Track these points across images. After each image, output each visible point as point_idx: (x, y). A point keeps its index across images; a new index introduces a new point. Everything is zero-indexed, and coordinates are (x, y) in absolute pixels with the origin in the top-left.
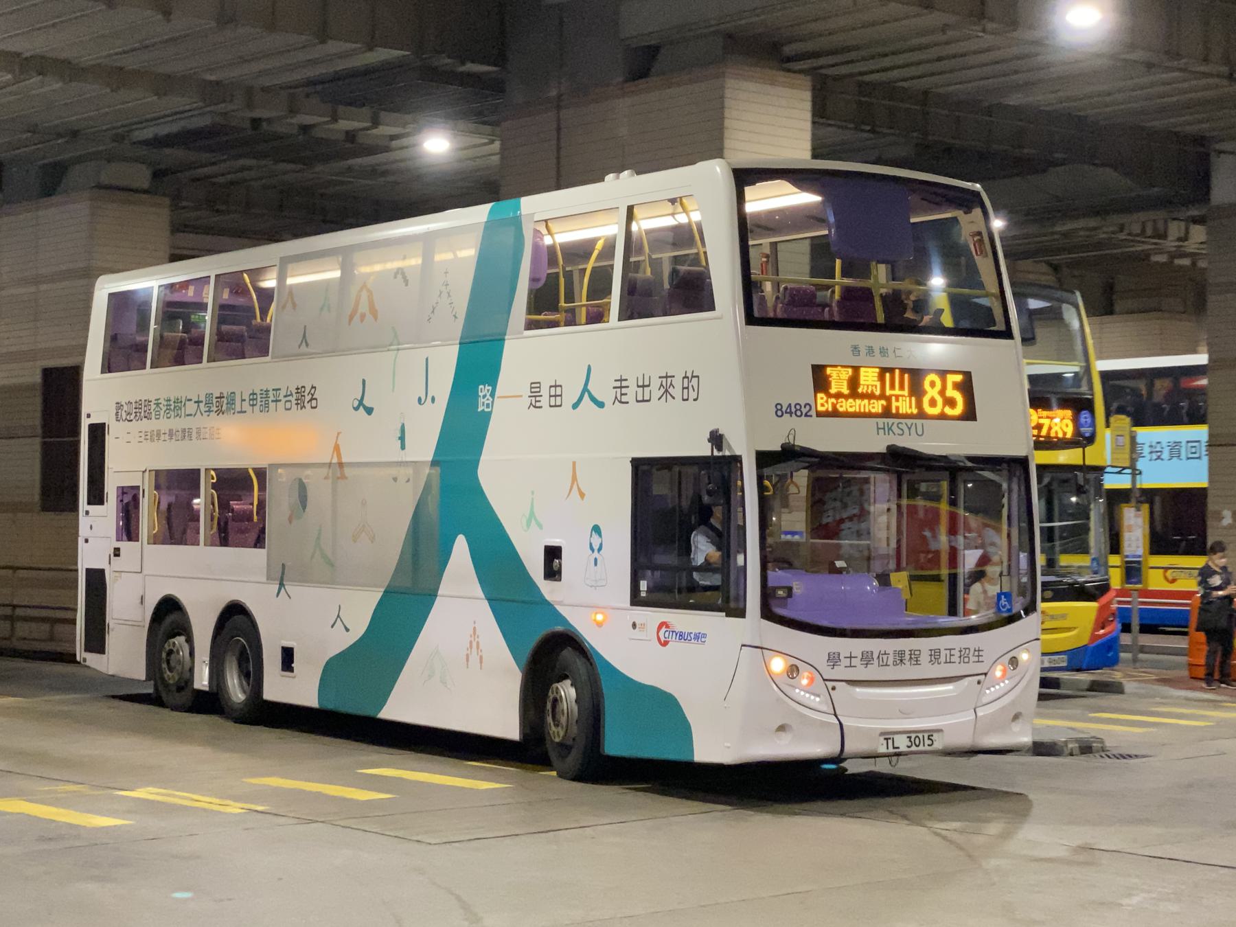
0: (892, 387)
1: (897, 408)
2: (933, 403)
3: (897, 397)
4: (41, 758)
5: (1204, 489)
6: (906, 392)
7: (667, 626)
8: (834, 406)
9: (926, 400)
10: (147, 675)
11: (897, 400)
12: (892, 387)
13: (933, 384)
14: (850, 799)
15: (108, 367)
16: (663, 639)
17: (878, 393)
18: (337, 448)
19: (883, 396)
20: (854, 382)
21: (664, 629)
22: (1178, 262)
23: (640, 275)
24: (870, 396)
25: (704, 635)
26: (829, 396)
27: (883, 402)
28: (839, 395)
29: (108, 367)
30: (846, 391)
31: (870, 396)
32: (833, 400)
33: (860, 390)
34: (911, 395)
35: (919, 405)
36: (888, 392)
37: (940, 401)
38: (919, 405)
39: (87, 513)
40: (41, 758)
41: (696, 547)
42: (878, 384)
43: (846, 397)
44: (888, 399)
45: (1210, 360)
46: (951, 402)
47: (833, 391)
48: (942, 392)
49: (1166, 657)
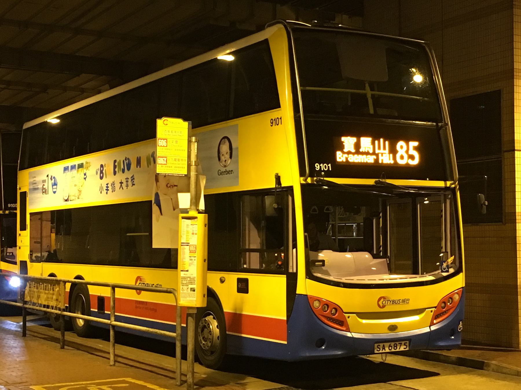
0: (379, 148)
1: (382, 160)
2: (402, 157)
3: (382, 154)
6: (387, 150)
7: (141, 280)
8: (347, 159)
9: (398, 156)
11: (382, 155)
12: (379, 148)
13: (402, 147)
14: (385, 381)
16: (381, 305)
17: (371, 151)
18: (278, 179)
19: (374, 153)
20: (357, 146)
21: (382, 300)
24: (367, 153)
25: (408, 300)
26: (344, 153)
27: (375, 157)
28: (349, 153)
30: (353, 151)
31: (367, 153)
32: (346, 155)
33: (361, 150)
34: (389, 153)
35: (394, 158)
37: (406, 156)
38: (394, 158)
39: (20, 235)
41: (181, 236)
42: (372, 147)
43: (354, 154)
44: (377, 155)
46: (412, 157)
47: (345, 150)
48: (407, 152)
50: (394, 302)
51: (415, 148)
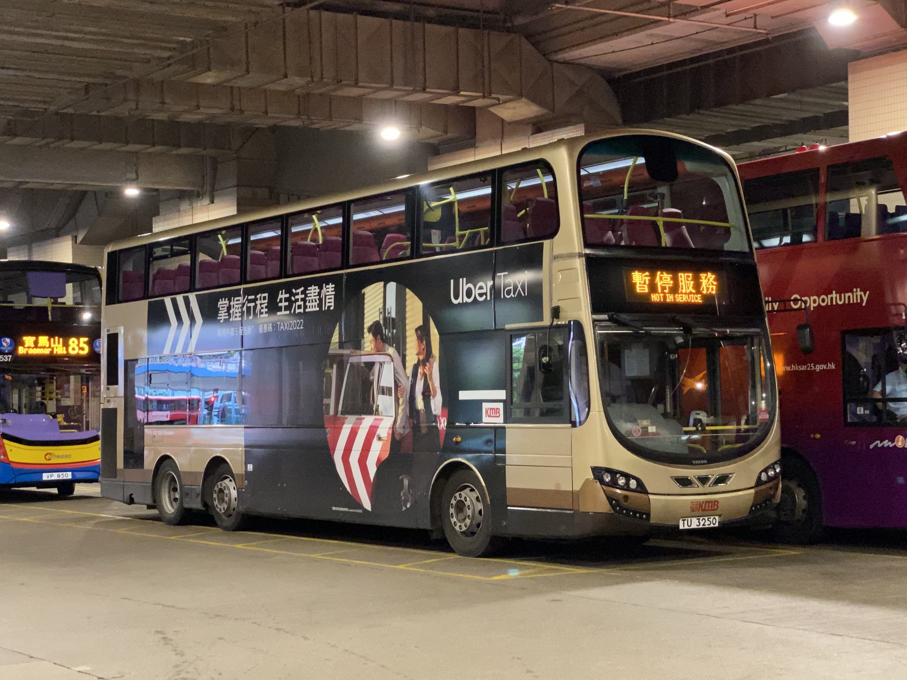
4: (889, 569)
5: (143, 467)
10: (849, 202)
15: (107, 304)
19: (50, 347)
22: (253, 297)
23: (728, 246)
24: (44, 347)
28: (29, 347)
29: (107, 304)
31: (44, 347)
35: (67, 350)
36: (52, 345)
37: (77, 348)
38: (67, 350)
40: (889, 569)
44: (53, 349)
45: (791, 239)
46: (83, 349)
48: (78, 345)
49: (542, 144)
50: (58, 457)
51: (85, 343)
